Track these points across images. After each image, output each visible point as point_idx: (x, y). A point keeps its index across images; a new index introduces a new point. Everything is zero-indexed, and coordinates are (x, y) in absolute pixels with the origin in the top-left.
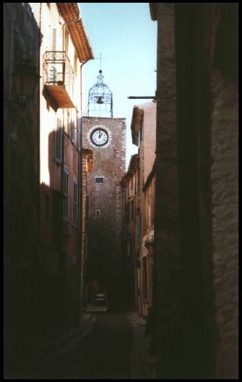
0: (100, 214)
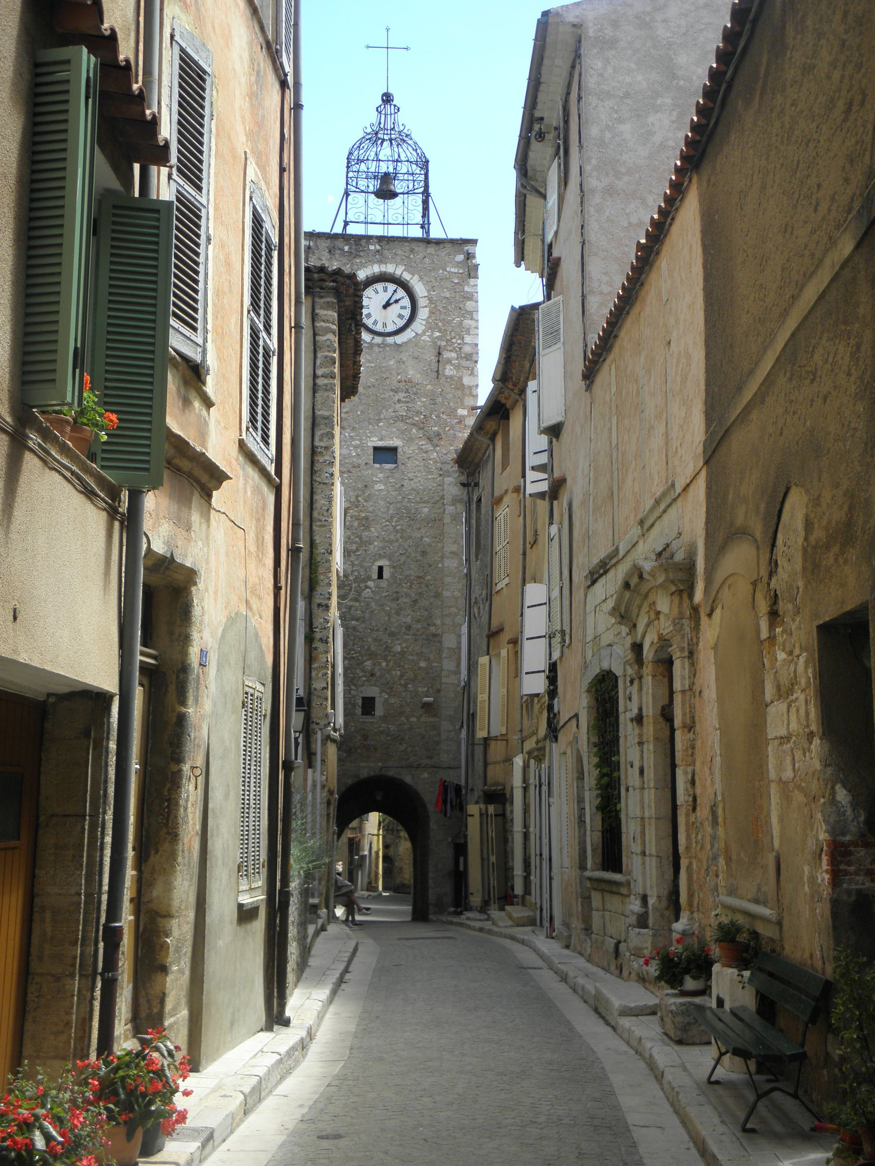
0: (386, 574)
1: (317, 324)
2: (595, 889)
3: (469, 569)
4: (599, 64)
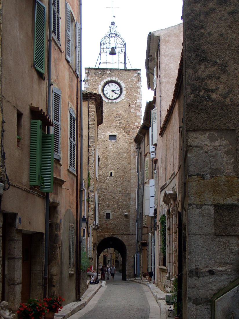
1: (89, 109)
2: (161, 271)
3: (138, 174)
4: (165, 47)
